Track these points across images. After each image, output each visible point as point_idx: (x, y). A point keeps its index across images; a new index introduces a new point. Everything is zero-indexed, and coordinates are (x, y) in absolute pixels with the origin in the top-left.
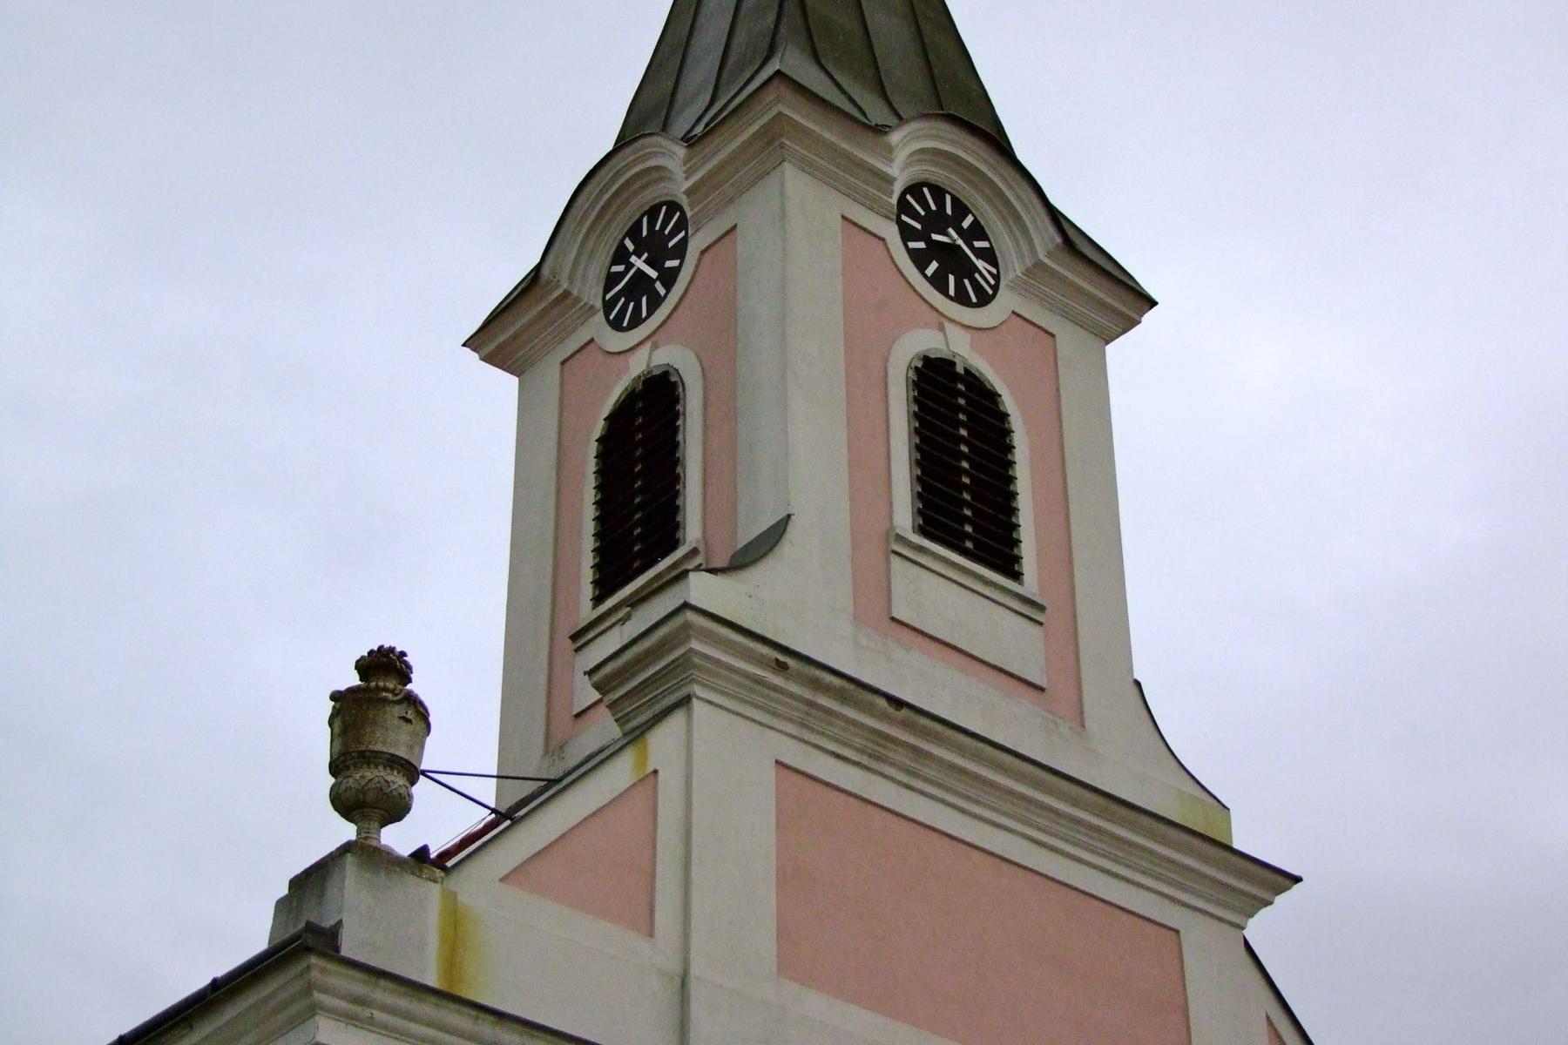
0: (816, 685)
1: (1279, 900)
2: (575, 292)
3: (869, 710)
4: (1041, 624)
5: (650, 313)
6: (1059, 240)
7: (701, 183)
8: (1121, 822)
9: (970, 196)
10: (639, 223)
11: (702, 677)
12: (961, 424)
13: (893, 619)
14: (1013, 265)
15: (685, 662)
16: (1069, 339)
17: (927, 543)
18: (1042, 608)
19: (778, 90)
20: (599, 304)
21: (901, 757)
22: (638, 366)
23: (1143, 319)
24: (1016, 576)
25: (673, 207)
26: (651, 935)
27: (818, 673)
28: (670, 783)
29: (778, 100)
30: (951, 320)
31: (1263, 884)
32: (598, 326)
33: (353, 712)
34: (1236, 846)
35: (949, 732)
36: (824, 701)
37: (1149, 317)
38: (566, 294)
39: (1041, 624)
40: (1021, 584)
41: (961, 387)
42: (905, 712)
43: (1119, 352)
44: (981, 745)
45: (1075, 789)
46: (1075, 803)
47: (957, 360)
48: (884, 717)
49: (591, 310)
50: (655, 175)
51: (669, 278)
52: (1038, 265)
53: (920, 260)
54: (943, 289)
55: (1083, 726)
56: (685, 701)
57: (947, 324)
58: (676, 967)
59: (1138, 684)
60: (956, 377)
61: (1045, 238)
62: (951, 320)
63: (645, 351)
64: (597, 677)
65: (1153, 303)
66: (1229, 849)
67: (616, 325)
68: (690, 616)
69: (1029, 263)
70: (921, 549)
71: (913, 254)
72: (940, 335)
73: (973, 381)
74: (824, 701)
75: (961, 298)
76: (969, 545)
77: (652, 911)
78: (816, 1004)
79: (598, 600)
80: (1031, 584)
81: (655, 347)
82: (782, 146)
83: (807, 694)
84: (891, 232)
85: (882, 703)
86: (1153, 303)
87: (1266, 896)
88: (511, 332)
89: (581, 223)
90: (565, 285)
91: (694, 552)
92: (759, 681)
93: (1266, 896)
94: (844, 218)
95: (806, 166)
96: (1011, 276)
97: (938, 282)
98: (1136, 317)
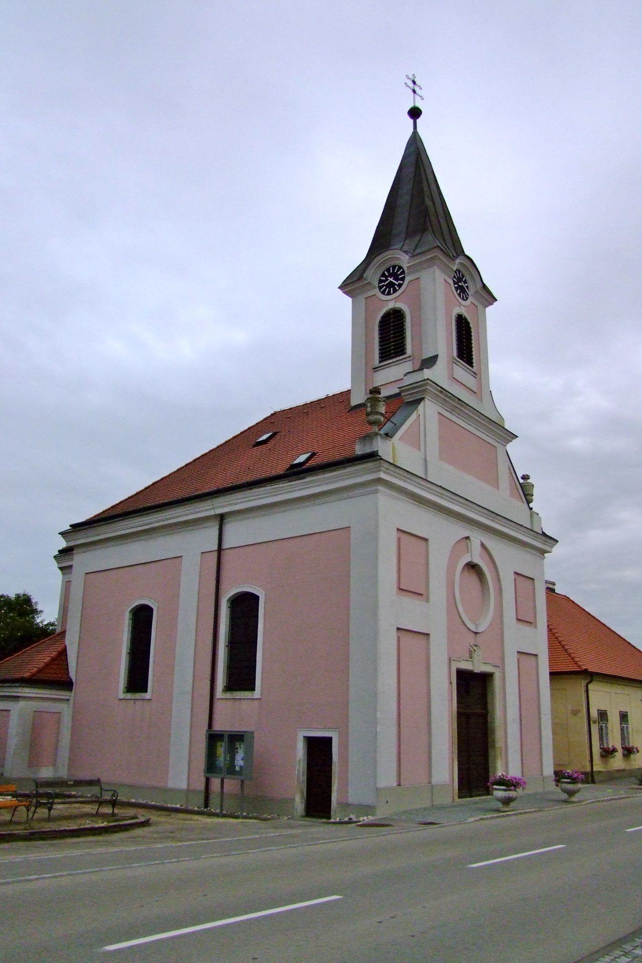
0: (447, 396)
1: (514, 440)
2: (371, 283)
3: (454, 401)
4: (476, 378)
7: (411, 266)
8: (490, 424)
9: (465, 273)
11: (428, 392)
12: (463, 330)
13: (454, 378)
15: (425, 390)
16: (480, 307)
17: (459, 360)
19: (438, 250)
20: (377, 286)
21: (457, 410)
22: (391, 305)
23: (495, 303)
24: (472, 367)
27: (447, 393)
28: (422, 417)
29: (436, 252)
31: (510, 437)
32: (376, 291)
34: (505, 427)
36: (447, 399)
37: (496, 303)
38: (370, 282)
39: (476, 378)
40: (472, 367)
43: (489, 310)
45: (484, 417)
46: (484, 420)
48: (456, 403)
49: (375, 287)
51: (400, 286)
52: (477, 291)
53: (456, 289)
54: (460, 297)
56: (423, 399)
57: (461, 306)
58: (423, 457)
59: (491, 391)
61: (479, 285)
63: (393, 302)
65: (496, 300)
66: (504, 428)
67: (383, 293)
68: (428, 381)
71: (455, 287)
72: (459, 308)
73: (465, 319)
74: (447, 399)
75: (463, 299)
78: (445, 466)
79: (380, 362)
80: (474, 369)
81: (396, 302)
83: (444, 397)
85: (457, 400)
86: (496, 300)
87: (510, 439)
89: (374, 265)
90: (369, 281)
91: (410, 357)
92: (438, 396)
93: (510, 439)
95: (438, 266)
97: (459, 295)
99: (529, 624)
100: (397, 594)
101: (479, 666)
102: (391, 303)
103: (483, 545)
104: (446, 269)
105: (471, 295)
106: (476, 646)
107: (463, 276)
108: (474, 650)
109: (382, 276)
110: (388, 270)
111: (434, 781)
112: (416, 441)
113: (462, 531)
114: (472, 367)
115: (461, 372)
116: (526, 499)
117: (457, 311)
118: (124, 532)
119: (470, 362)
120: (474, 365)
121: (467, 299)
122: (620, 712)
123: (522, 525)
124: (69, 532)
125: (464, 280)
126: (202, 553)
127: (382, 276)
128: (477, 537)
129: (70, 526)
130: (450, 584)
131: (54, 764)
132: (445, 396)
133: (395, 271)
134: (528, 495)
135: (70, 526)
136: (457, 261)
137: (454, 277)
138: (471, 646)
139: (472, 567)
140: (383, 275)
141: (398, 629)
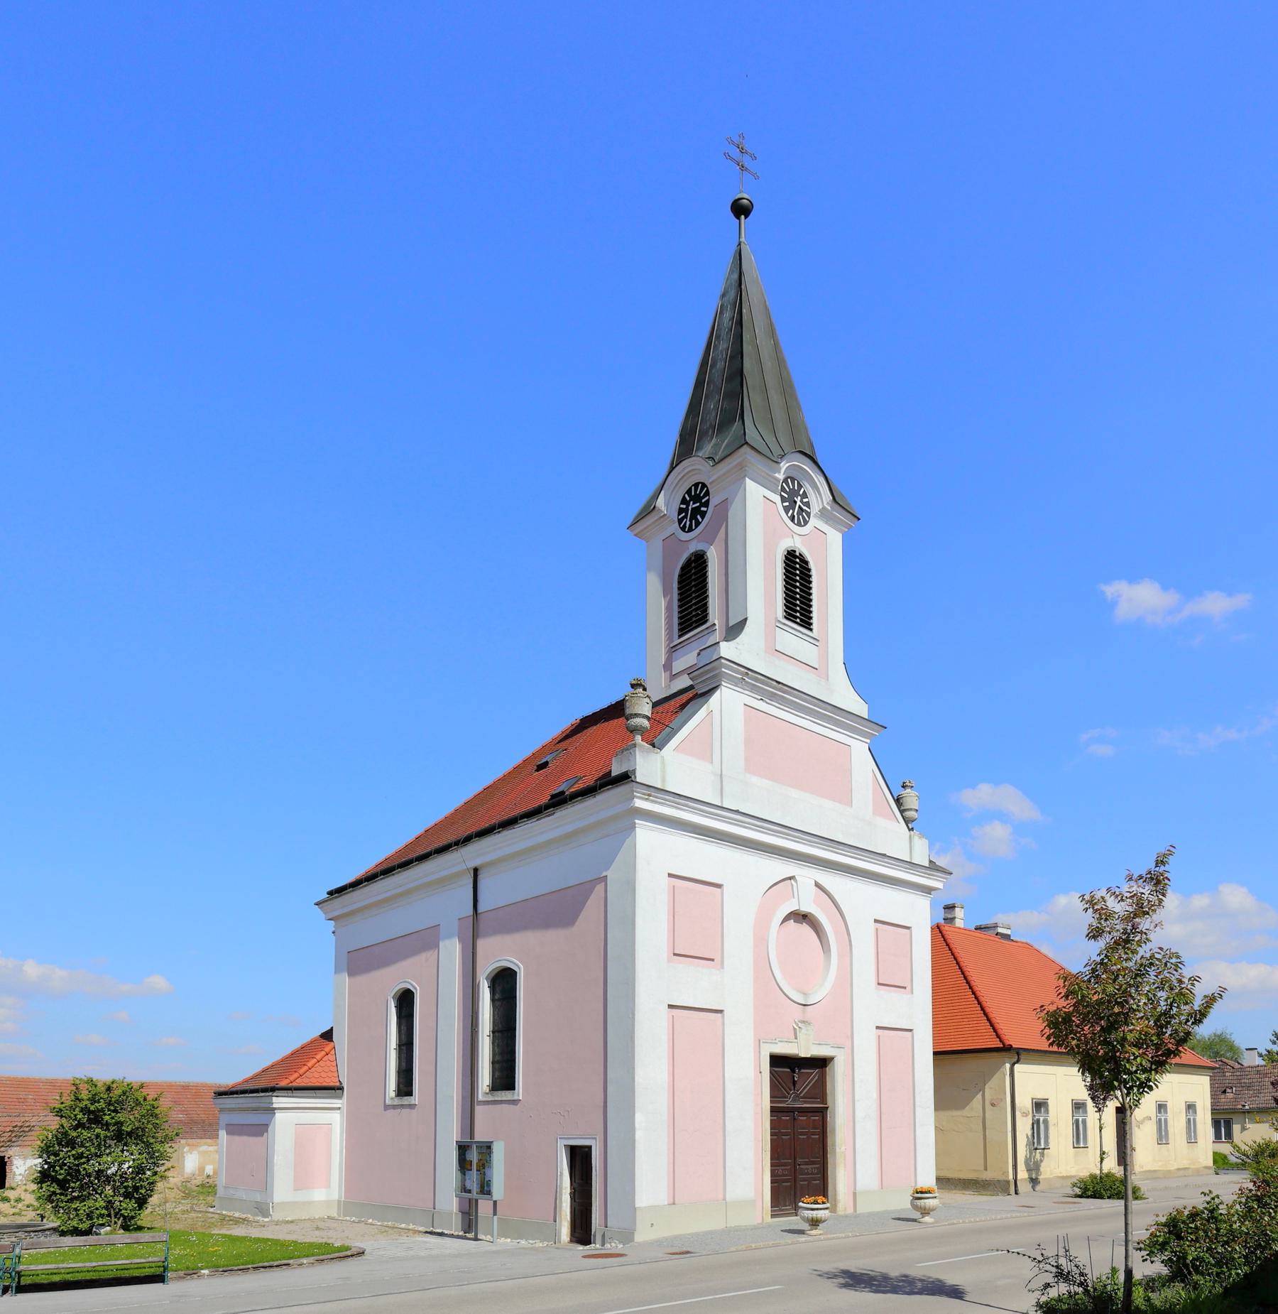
0: (756, 680)
5: (696, 527)
6: (831, 498)
10: (690, 488)
14: (815, 508)
18: (818, 640)
25: (704, 485)
26: (712, 763)
27: (756, 675)
28: (716, 714)
30: (796, 534)
33: (1060, 1020)
35: (792, 691)
40: (811, 630)
41: (798, 560)
42: (780, 685)
44: (799, 693)
47: (797, 550)
50: (696, 472)
52: (824, 508)
55: (828, 680)
57: (795, 535)
60: (796, 557)
62: (796, 534)
64: (691, 676)
69: (821, 507)
70: (784, 624)
75: (799, 524)
76: (798, 620)
77: (712, 755)
78: (755, 780)
80: (815, 634)
82: (746, 470)
84: (777, 499)
85: (775, 683)
88: (645, 526)
94: (764, 497)
96: (815, 512)
98: (952, 916)
99: (903, 990)
100: (669, 961)
101: (804, 1048)
102: (692, 543)
103: (817, 885)
104: (767, 483)
105: (815, 516)
106: (803, 1022)
107: (800, 486)
108: (800, 1028)
109: (682, 503)
110: (689, 492)
111: (728, 1197)
112: (704, 750)
113: (779, 868)
114: (811, 630)
115: (791, 639)
116: (902, 815)
117: (787, 544)
118: (380, 897)
119: (806, 623)
120: (814, 627)
121: (806, 523)
122: (1186, 1102)
123: (884, 855)
124: (326, 901)
125: (801, 493)
126: (459, 919)
127: (682, 503)
128: (807, 876)
129: (328, 893)
130: (760, 942)
131: (328, 1186)
132: (751, 679)
133: (698, 492)
134: (905, 810)
135: (328, 893)
136: (784, 465)
137: (783, 489)
138: (795, 1023)
139: (802, 917)
140: (684, 501)
141: (670, 1006)
